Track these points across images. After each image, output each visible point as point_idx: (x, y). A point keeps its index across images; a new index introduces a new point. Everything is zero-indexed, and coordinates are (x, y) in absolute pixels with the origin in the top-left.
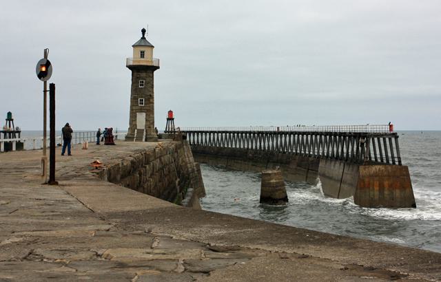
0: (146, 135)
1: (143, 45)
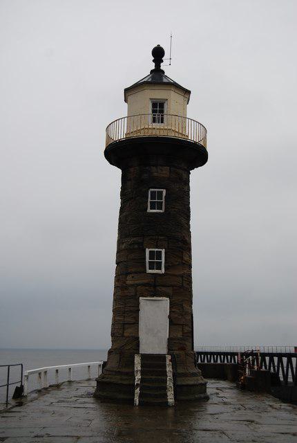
0: (174, 375)
1: (156, 86)
